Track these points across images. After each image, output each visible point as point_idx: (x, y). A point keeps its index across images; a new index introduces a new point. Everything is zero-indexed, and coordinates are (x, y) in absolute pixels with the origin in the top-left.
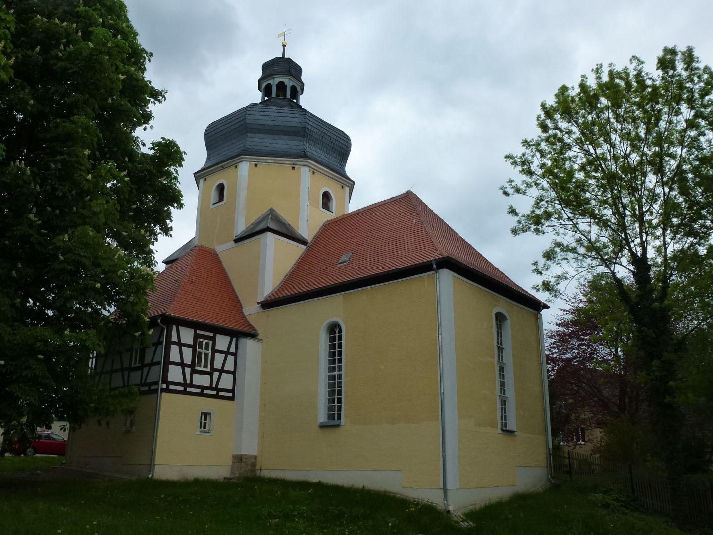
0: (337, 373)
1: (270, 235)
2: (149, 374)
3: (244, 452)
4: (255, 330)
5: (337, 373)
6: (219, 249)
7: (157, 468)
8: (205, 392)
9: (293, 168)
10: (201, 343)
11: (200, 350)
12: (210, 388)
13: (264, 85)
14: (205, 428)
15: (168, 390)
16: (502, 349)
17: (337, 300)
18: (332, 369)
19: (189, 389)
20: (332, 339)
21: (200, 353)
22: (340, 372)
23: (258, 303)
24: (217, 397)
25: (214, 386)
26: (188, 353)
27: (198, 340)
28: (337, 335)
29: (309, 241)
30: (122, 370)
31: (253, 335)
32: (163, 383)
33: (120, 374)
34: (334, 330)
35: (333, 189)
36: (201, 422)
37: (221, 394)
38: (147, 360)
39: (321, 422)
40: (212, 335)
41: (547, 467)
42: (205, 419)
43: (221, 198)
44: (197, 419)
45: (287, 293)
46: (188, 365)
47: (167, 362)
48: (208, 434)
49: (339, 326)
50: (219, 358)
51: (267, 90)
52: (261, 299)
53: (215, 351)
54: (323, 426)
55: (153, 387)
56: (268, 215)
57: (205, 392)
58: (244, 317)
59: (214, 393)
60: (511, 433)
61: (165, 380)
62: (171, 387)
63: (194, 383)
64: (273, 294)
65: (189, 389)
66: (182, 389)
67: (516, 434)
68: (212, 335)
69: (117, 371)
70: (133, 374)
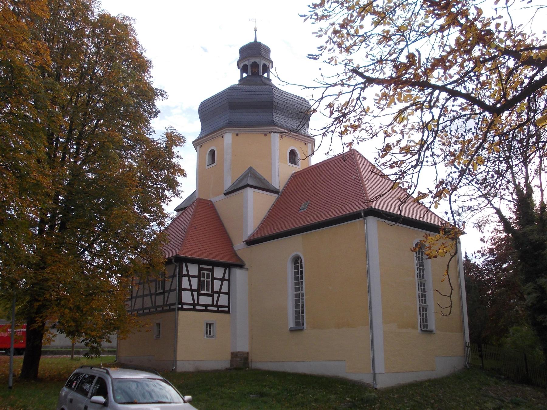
0: (300, 292)
1: (250, 191)
3: (238, 350)
4: (242, 261)
5: (300, 292)
6: (214, 199)
7: (178, 363)
8: (209, 308)
9: (266, 135)
10: (203, 274)
11: (203, 279)
12: (212, 305)
13: (242, 65)
14: (210, 333)
15: (182, 309)
16: (423, 270)
17: (298, 237)
18: (297, 289)
19: (197, 307)
20: (296, 268)
21: (203, 281)
22: (302, 292)
23: (244, 242)
24: (218, 311)
25: (215, 304)
26: (194, 281)
27: (202, 272)
28: (299, 264)
29: (281, 190)
30: (151, 294)
31: (241, 266)
32: (179, 304)
33: (149, 297)
34: (297, 260)
35: (297, 146)
36: (207, 330)
37: (220, 309)
38: (167, 288)
39: (290, 328)
40: (211, 267)
41: (465, 356)
42: (210, 327)
43: (213, 161)
44: (204, 328)
45: (266, 233)
46: (195, 290)
47: (181, 289)
48: (212, 338)
49: (300, 258)
50: (217, 284)
51: (244, 69)
52: (245, 239)
53: (214, 279)
54: (292, 330)
55: (172, 307)
56: (248, 173)
57: (209, 308)
58: (234, 250)
59: (215, 309)
60: (431, 332)
61: (180, 302)
62: (185, 307)
63: (200, 303)
64: (254, 234)
65: (197, 307)
66: (192, 307)
67: (435, 332)
68: (211, 267)
69: (147, 295)
70: (158, 297)
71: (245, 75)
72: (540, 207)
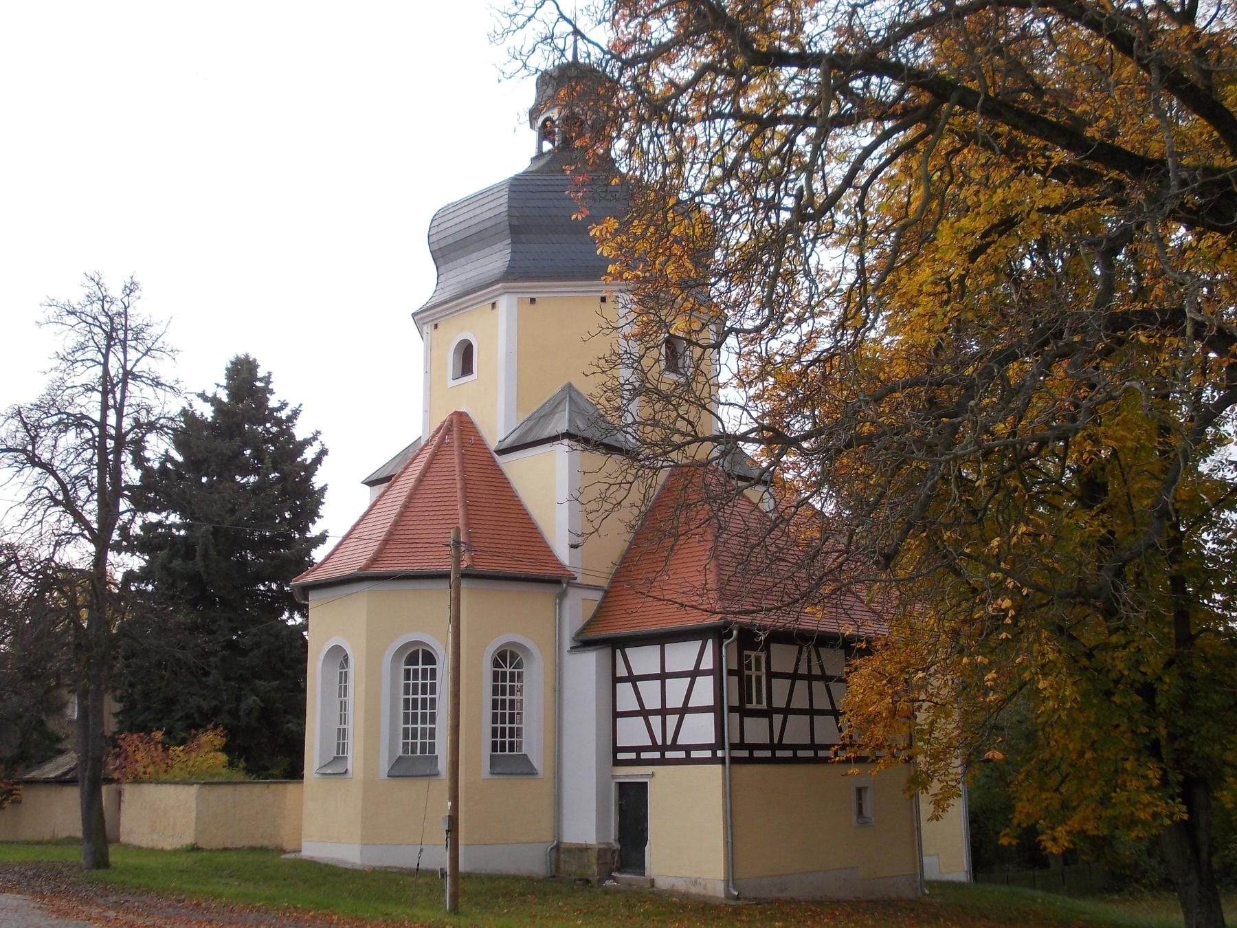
2: (567, 693)
8: (644, 755)
12: (654, 748)
21: (750, 677)
22: (433, 726)
50: (779, 687)
57: (644, 755)
71: (547, 146)
72: (142, 553)
